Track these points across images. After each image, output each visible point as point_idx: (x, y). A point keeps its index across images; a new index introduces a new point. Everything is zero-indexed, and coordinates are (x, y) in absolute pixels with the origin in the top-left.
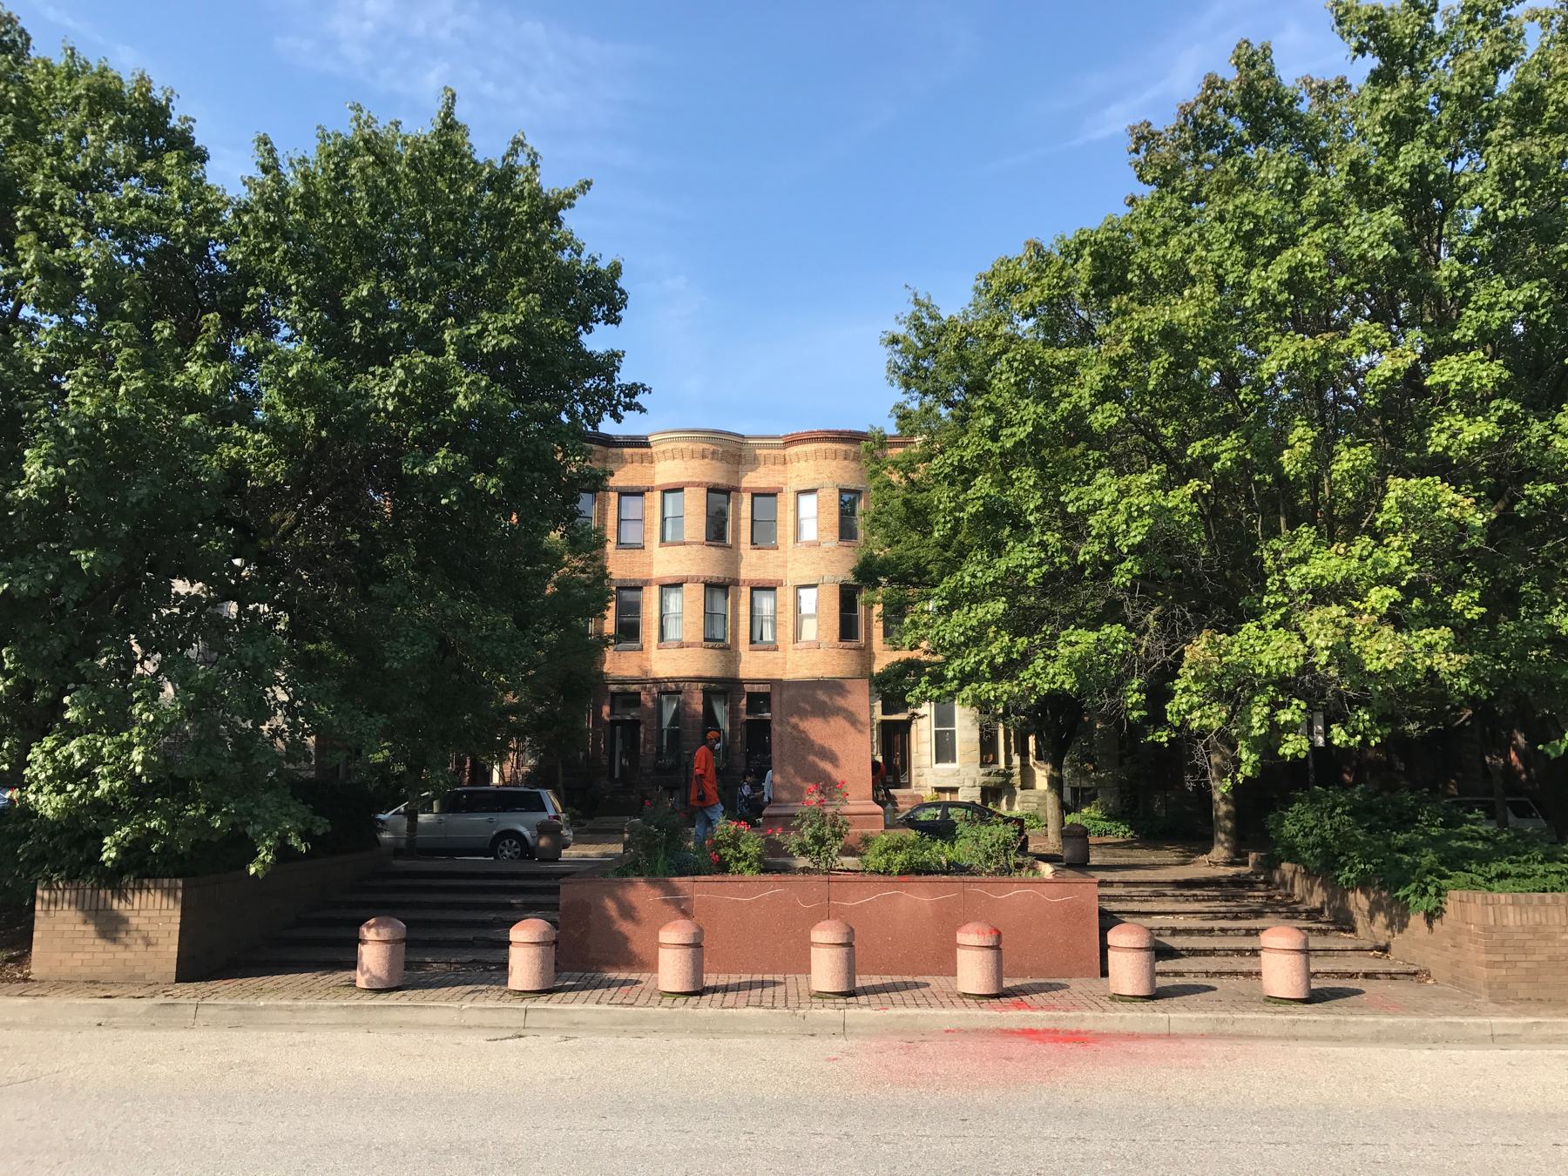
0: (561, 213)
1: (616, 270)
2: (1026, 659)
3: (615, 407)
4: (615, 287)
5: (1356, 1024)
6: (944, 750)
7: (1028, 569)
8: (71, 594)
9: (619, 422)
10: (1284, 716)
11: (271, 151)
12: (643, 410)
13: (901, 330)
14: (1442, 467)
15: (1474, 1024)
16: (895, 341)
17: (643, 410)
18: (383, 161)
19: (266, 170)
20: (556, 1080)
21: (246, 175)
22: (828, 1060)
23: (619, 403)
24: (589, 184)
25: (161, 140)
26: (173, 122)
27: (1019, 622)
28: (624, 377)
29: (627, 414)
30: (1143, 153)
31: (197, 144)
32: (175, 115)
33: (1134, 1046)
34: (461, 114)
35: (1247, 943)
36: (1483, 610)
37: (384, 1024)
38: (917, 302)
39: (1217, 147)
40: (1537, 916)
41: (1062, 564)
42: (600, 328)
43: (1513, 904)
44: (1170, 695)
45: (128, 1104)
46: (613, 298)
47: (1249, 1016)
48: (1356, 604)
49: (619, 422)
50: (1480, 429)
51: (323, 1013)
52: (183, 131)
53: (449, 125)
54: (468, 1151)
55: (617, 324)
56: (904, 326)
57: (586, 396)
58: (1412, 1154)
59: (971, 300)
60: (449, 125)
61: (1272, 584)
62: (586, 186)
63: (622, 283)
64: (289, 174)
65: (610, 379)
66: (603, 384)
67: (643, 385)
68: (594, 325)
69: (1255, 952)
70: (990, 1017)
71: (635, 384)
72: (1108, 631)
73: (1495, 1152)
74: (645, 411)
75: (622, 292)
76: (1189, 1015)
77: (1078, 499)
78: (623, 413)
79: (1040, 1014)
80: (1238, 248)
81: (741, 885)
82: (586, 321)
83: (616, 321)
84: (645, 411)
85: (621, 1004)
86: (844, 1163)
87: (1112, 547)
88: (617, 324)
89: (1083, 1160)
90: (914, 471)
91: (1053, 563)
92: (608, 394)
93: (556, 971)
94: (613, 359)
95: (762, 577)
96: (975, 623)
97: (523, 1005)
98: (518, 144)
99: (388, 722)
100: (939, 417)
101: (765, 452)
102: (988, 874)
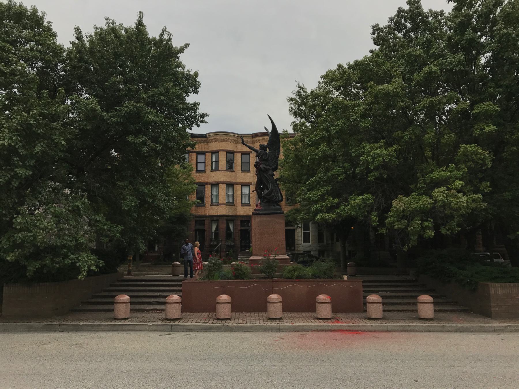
0: (179, 55)
1: (196, 74)
2: (338, 206)
3: (197, 122)
4: (196, 81)
5: (449, 326)
6: (306, 239)
7: (339, 175)
8: (15, 184)
9: (199, 127)
10: (426, 224)
11: (80, 33)
12: (207, 123)
13: (294, 96)
14: (475, 141)
15: (489, 326)
16: (291, 100)
17: (207, 123)
18: (118, 36)
19: (78, 38)
20: (184, 348)
21: (72, 40)
22: (275, 341)
23: (198, 120)
24: (188, 45)
25: (41, 30)
26: (45, 24)
27: (335, 194)
28: (200, 111)
29: (201, 124)
30: (376, 34)
31: (53, 31)
32: (46, 21)
33: (376, 334)
34: (145, 21)
35: (411, 301)
36: (491, 189)
37: (124, 330)
38: (300, 87)
39: (401, 33)
40: (504, 291)
41: (350, 173)
42: (191, 95)
43: (500, 287)
44: (386, 218)
45: (38, 358)
46: (195, 84)
47: (415, 324)
48: (449, 186)
49: (199, 127)
50: (490, 128)
51: (103, 327)
52: (48, 27)
53: (140, 23)
54: (156, 372)
55: (197, 93)
56: (295, 95)
57: (187, 118)
58: (474, 369)
59: (317, 86)
60: (140, 23)
61: (420, 181)
62: (187, 46)
63: (198, 79)
64: (86, 39)
65: (195, 112)
66: (193, 114)
67: (206, 114)
68: (189, 94)
69: (415, 304)
70: (328, 326)
71: (203, 113)
72: (366, 196)
73: (502, 368)
74: (207, 123)
75: (199, 82)
76: (395, 324)
77: (356, 151)
78: (200, 124)
79: (345, 324)
80: (409, 67)
81: (243, 283)
82: (187, 93)
83: (197, 92)
84: (207, 123)
85: (204, 323)
86: (285, 375)
87: (367, 168)
88: (197, 93)
89: (365, 373)
90: (297, 145)
91: (346, 173)
92: (195, 117)
93: (181, 312)
94: (196, 105)
95: (245, 182)
96: (320, 193)
97: (171, 324)
98: (164, 31)
99: (123, 228)
100: (306, 126)
101: (246, 139)
102: (325, 279)
